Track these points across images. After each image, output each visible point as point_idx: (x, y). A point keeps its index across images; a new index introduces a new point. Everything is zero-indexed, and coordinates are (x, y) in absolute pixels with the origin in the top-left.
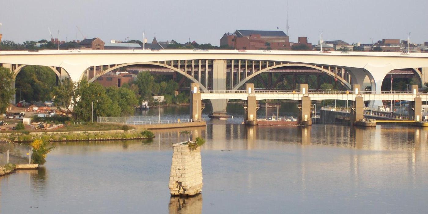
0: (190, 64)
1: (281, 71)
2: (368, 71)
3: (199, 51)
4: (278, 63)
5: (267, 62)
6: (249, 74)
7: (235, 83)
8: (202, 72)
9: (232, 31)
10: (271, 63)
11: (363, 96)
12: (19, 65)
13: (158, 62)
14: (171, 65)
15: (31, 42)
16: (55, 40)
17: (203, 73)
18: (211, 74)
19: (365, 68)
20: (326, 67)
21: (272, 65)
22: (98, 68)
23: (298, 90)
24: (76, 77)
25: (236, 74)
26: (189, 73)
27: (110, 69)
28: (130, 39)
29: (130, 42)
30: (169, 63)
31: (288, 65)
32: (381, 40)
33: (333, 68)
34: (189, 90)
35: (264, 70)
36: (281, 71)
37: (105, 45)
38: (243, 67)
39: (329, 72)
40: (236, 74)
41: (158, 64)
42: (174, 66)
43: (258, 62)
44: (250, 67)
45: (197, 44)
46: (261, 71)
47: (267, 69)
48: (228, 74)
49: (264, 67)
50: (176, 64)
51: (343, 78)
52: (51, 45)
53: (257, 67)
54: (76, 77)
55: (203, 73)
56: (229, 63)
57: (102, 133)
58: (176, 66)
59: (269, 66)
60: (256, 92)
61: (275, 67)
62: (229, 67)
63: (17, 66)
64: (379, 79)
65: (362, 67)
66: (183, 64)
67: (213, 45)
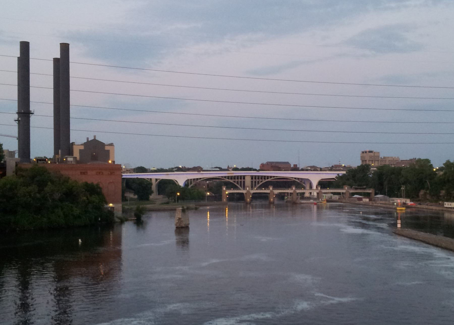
0: (235, 177)
1: (276, 180)
2: (310, 179)
3: (255, 172)
4: (274, 177)
5: (266, 177)
6: (261, 182)
7: (255, 185)
8: (258, 181)
9: (265, 162)
10: (271, 177)
11: (250, 191)
12: (159, 179)
13: (224, 177)
14: (226, 178)
15: (432, 165)
16: (184, 167)
17: (241, 182)
18: (244, 182)
19: (309, 179)
20: (295, 178)
21: (271, 178)
22: (194, 179)
23: (269, 189)
24: (181, 183)
25: (255, 182)
26: (235, 182)
27: (199, 180)
28: (215, 167)
29: (215, 168)
30: (225, 177)
31: (278, 177)
32: (333, 165)
33: (298, 179)
34: (273, 188)
35: (268, 180)
36: (276, 180)
37: (203, 169)
38: (258, 179)
39: (297, 180)
40: (255, 182)
41: (219, 178)
42: (228, 179)
43: (265, 176)
44: (262, 178)
45: (238, 169)
46: (267, 180)
47: (269, 180)
48: (252, 182)
49: (268, 178)
50: (228, 177)
51: (239, 184)
52: (171, 170)
53: (265, 179)
54: (181, 183)
55: (241, 182)
56: (252, 177)
57: (448, 205)
58: (228, 178)
59: (270, 178)
60: (274, 189)
61: (272, 178)
62: (252, 179)
63: (158, 179)
64: (315, 184)
65: (307, 178)
66: (231, 178)
67: (258, 169)
